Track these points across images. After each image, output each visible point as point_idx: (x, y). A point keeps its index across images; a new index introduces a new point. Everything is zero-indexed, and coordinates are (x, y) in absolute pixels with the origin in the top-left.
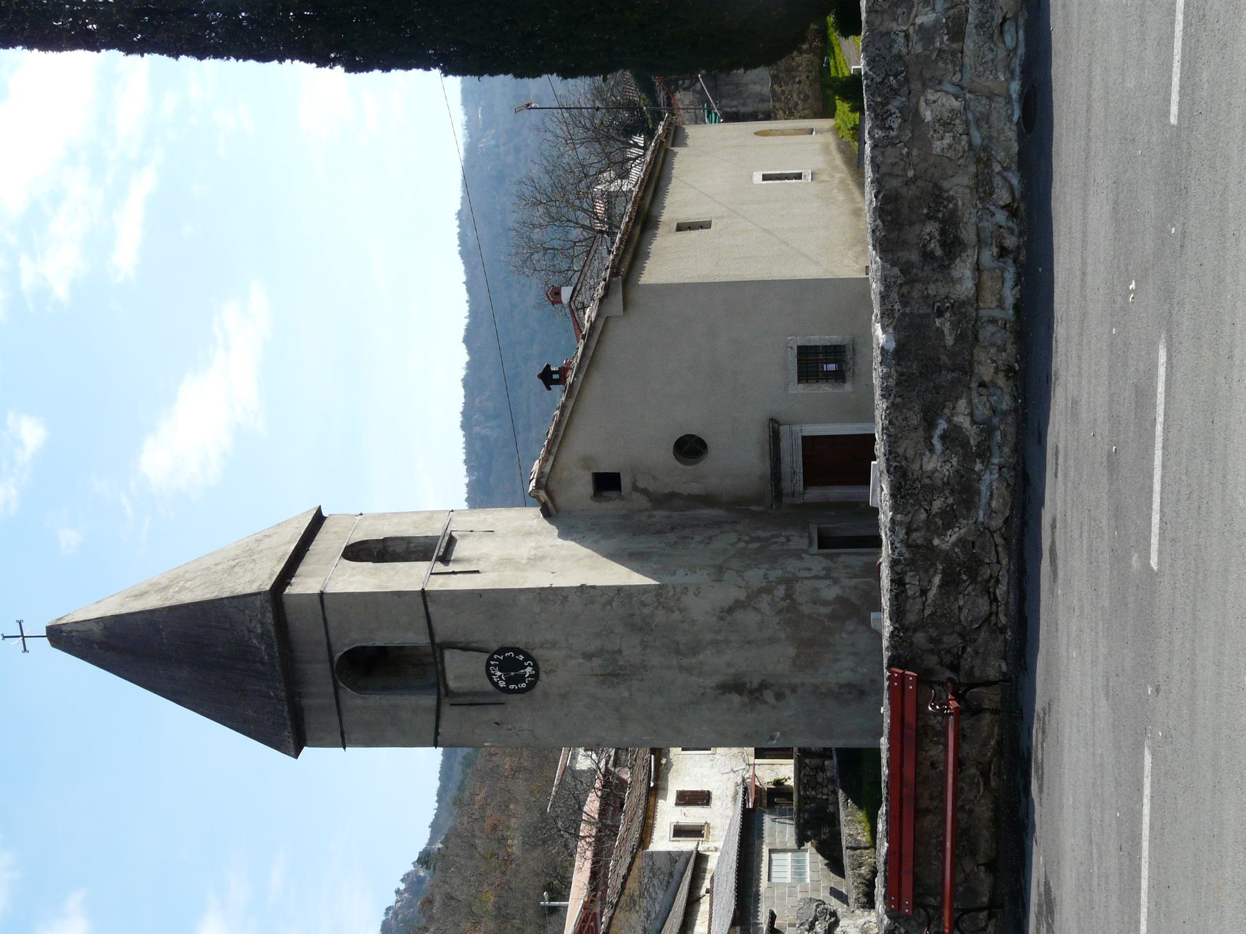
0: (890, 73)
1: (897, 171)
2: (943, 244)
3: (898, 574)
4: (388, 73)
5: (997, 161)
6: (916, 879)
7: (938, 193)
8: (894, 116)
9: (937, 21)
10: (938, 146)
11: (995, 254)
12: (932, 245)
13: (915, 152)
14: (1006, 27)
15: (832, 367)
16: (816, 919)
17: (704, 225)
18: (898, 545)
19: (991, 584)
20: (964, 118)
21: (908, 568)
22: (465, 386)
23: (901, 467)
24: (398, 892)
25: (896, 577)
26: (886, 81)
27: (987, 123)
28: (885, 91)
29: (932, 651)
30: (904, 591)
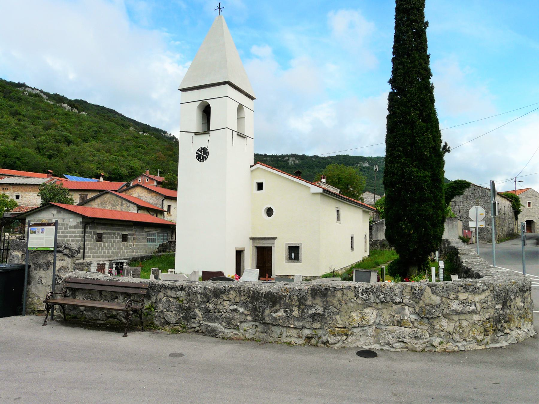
0: (385, 295)
1: (345, 297)
2: (314, 314)
3: (185, 288)
4: (391, 71)
5: (346, 338)
6: (77, 289)
7: (335, 313)
8: (367, 296)
9: (406, 315)
10: (354, 314)
11: (308, 335)
12: (313, 310)
13: (352, 305)
14: (402, 344)
15: (293, 257)
16: (70, 250)
17: (338, 218)
18: (195, 289)
19: (180, 324)
20: (365, 326)
21: (187, 293)
22: (302, 155)
23: (225, 292)
24: (170, 134)
25: (184, 288)
26: (382, 293)
27: (363, 335)
28: (378, 293)
29: (156, 299)
30: (179, 290)
